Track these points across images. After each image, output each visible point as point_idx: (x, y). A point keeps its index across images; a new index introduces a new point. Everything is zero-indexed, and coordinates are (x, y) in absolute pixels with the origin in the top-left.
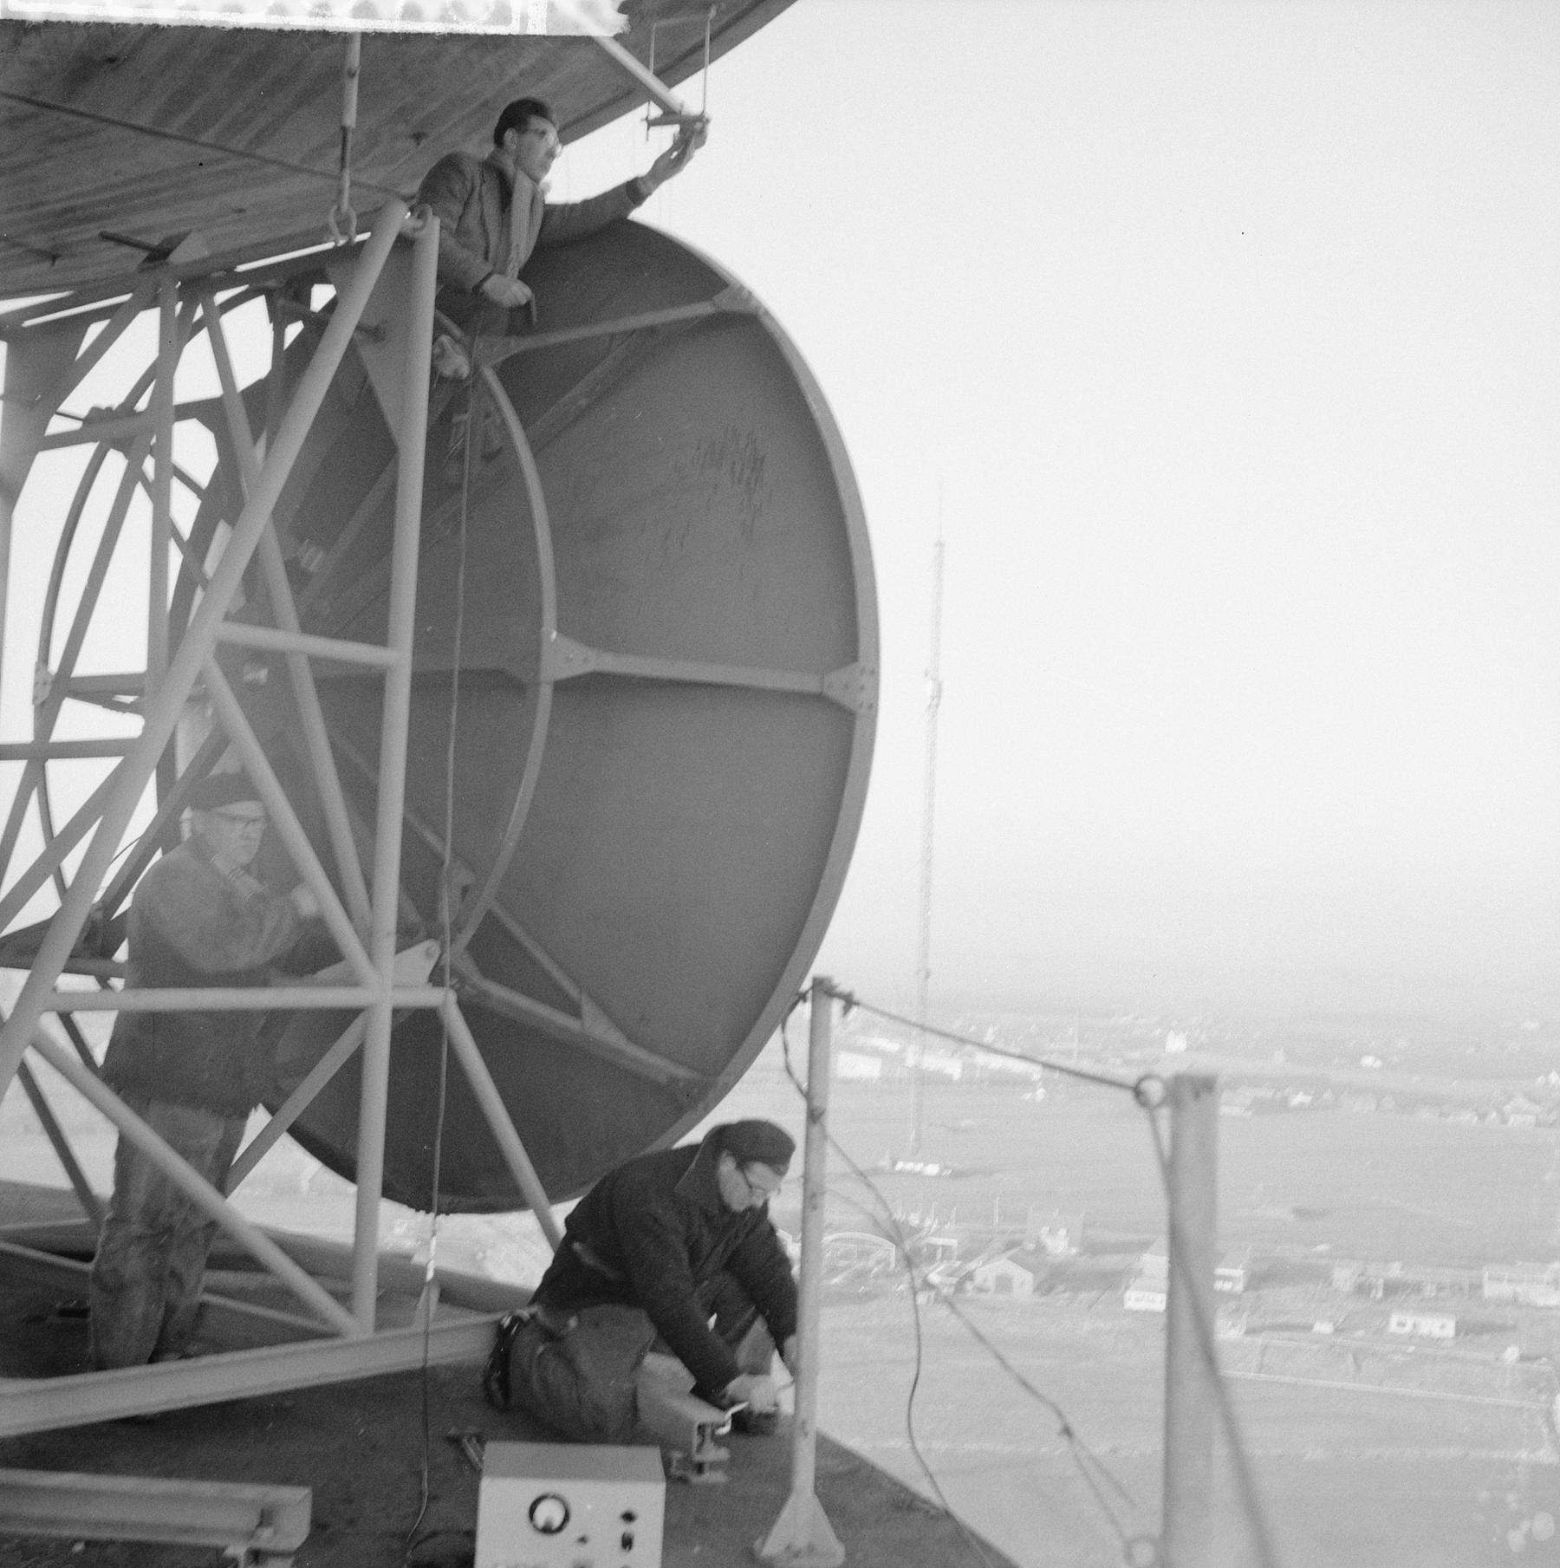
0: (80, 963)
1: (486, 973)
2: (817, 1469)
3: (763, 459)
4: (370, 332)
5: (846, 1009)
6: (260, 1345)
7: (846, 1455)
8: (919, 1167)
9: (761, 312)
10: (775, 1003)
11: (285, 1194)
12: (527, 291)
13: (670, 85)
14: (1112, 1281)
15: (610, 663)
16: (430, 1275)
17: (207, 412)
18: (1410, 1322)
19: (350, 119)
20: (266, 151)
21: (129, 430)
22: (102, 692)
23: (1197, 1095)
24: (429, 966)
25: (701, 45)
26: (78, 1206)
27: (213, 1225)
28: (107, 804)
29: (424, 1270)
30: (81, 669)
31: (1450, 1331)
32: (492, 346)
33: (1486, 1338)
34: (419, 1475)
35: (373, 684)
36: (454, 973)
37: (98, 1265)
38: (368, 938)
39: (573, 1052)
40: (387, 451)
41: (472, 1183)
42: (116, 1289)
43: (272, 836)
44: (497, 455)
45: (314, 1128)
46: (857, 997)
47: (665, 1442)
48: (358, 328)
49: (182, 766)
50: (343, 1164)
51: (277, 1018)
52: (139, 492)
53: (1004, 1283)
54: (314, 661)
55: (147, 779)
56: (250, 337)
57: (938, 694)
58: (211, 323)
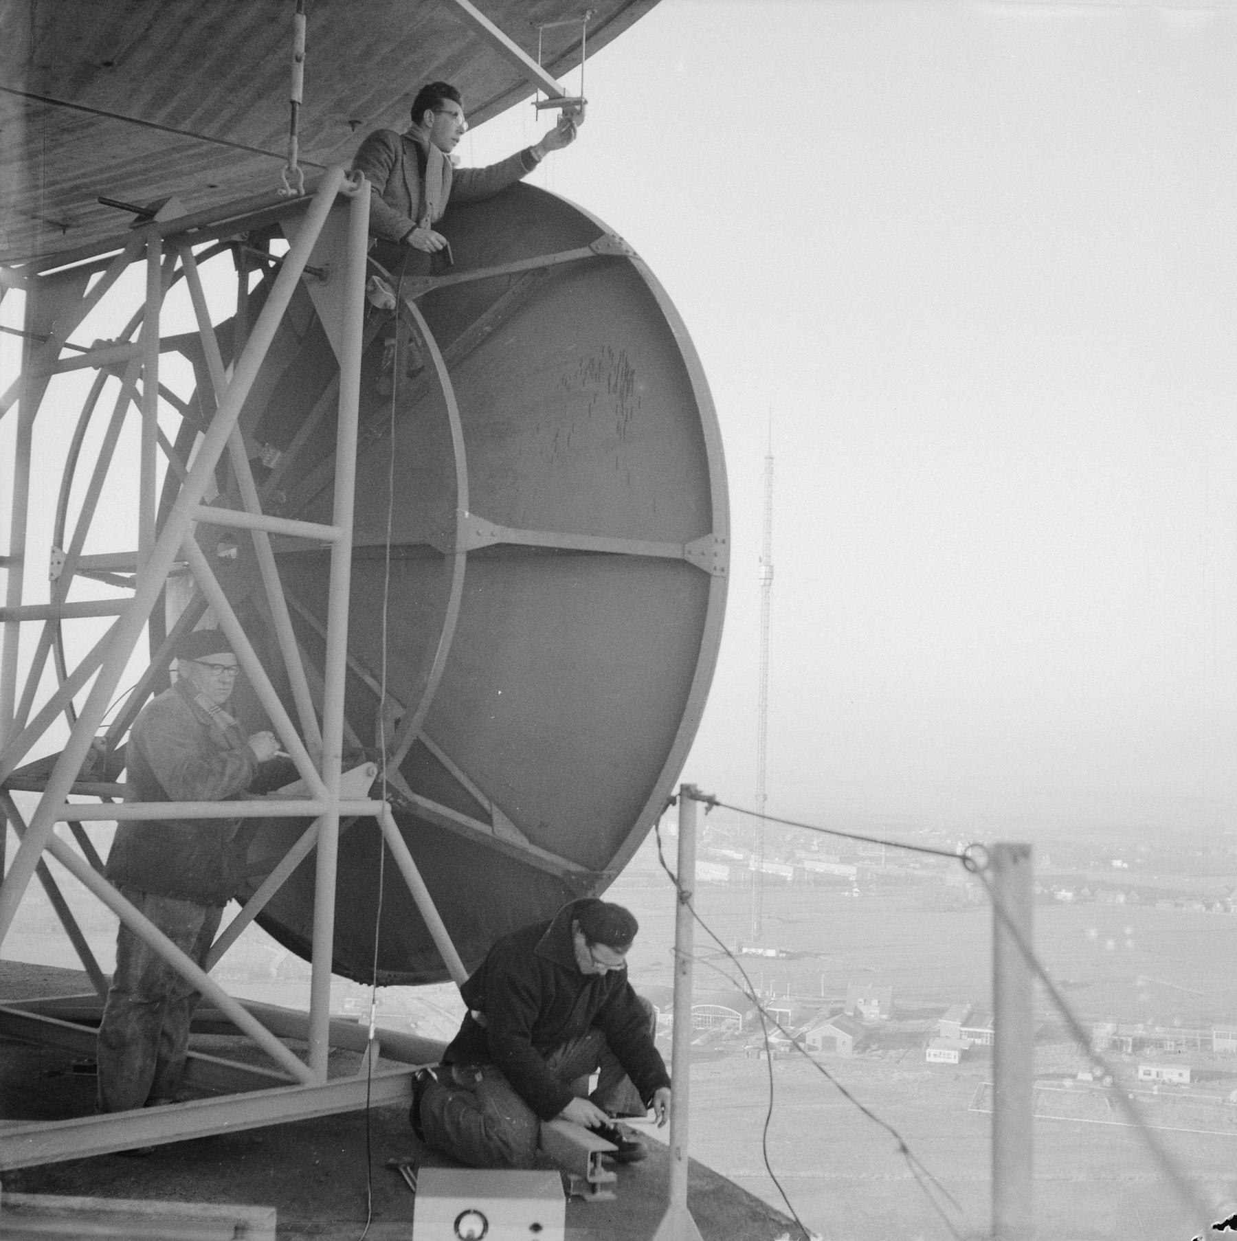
0: (87, 785)
1: (416, 790)
2: (689, 1187)
3: (633, 372)
4: (316, 273)
5: (708, 809)
6: (234, 1092)
7: (713, 1175)
8: (760, 951)
9: (631, 254)
10: (649, 808)
11: (254, 971)
12: (443, 239)
13: (556, 77)
14: (916, 1040)
15: (512, 536)
16: (372, 1036)
17: (187, 345)
18: (1154, 1071)
19: (298, 95)
20: (231, 138)
21: (122, 360)
22: (103, 569)
23: (1015, 861)
24: (370, 781)
25: (580, 43)
26: (87, 983)
27: (197, 994)
28: (108, 654)
29: (366, 1031)
30: (86, 551)
31: (1186, 1078)
32: (414, 284)
33: (1215, 1083)
34: (366, 1195)
35: (321, 557)
36: (390, 788)
37: (103, 1031)
38: (319, 760)
39: (488, 851)
40: (330, 368)
41: (406, 961)
42: (118, 1046)
43: (243, 681)
44: (419, 372)
45: (276, 915)
46: (718, 799)
47: (564, 1168)
48: (305, 270)
49: (170, 625)
50: (303, 948)
51: (250, 825)
52: (133, 408)
53: (829, 1043)
54: (275, 537)
55: (142, 627)
56: (220, 280)
57: (770, 577)
58: (189, 272)
